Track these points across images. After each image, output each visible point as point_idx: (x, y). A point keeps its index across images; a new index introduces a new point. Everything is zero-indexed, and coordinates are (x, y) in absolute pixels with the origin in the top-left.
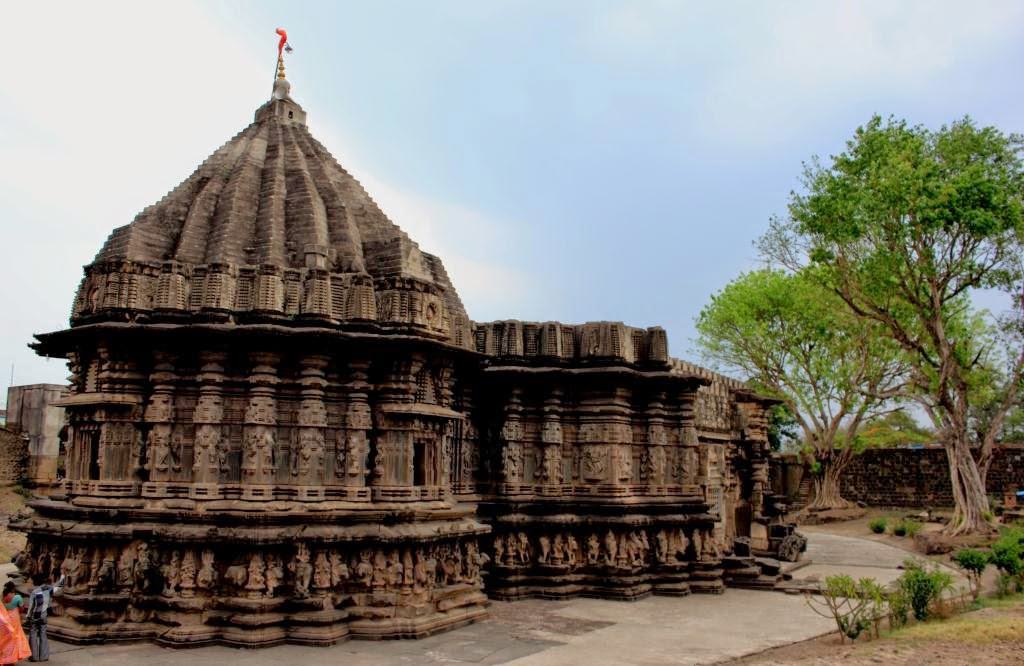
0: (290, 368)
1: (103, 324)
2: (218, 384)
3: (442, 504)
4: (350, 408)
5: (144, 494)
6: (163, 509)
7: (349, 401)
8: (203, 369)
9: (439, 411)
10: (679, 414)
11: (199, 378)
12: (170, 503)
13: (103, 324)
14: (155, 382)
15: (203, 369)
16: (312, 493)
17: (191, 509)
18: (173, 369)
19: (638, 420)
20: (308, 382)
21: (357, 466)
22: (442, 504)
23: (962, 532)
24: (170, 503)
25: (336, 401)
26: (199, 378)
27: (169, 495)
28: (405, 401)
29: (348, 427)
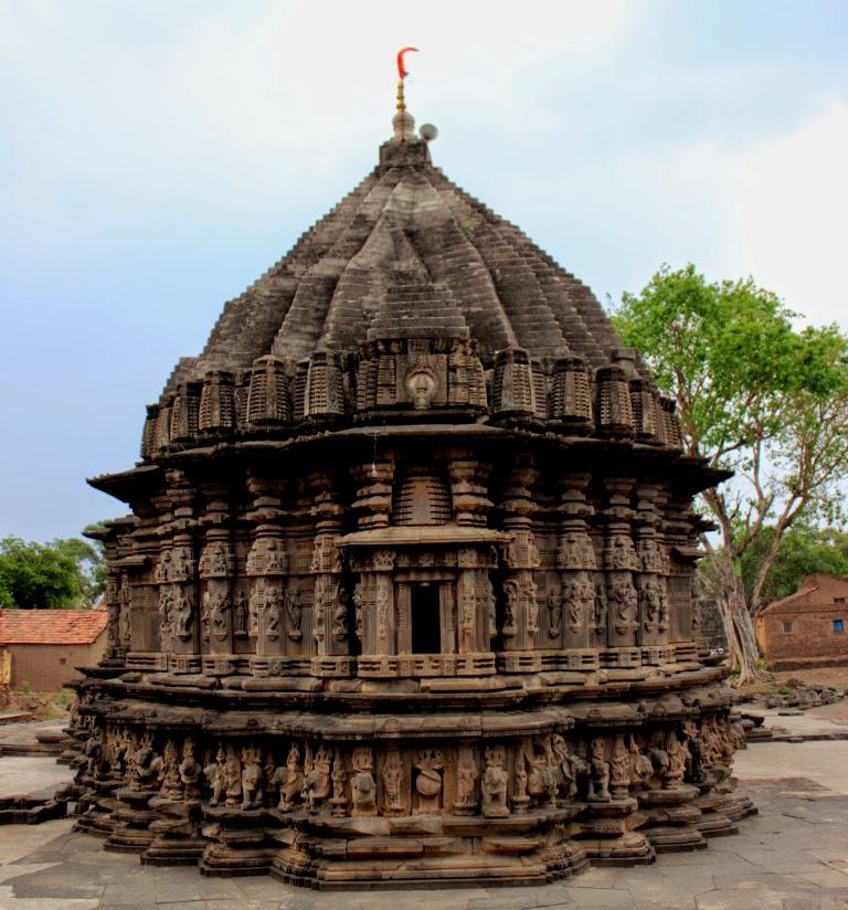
0: (550, 490)
1: (346, 432)
2: (334, 518)
3: (245, 681)
4: (613, 542)
5: (361, 673)
6: (540, 688)
7: (560, 531)
8: (564, 497)
9: (448, 533)
10: (561, 508)
11: (313, 511)
12: (551, 677)
13: (346, 432)
14: (254, 524)
15: (564, 497)
16: (587, 659)
17: (582, 684)
18: (628, 501)
19: (541, 523)
20: (515, 504)
21: (582, 623)
22: (245, 681)
23: (746, 681)
24: (551, 677)
25: (544, 533)
26: (313, 511)
27: (547, 667)
28: (371, 527)
29: (562, 567)
